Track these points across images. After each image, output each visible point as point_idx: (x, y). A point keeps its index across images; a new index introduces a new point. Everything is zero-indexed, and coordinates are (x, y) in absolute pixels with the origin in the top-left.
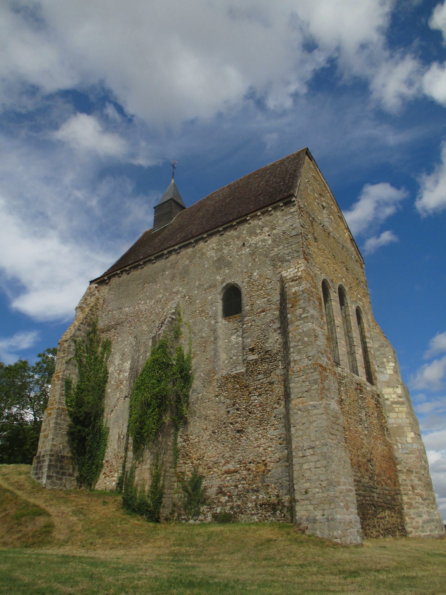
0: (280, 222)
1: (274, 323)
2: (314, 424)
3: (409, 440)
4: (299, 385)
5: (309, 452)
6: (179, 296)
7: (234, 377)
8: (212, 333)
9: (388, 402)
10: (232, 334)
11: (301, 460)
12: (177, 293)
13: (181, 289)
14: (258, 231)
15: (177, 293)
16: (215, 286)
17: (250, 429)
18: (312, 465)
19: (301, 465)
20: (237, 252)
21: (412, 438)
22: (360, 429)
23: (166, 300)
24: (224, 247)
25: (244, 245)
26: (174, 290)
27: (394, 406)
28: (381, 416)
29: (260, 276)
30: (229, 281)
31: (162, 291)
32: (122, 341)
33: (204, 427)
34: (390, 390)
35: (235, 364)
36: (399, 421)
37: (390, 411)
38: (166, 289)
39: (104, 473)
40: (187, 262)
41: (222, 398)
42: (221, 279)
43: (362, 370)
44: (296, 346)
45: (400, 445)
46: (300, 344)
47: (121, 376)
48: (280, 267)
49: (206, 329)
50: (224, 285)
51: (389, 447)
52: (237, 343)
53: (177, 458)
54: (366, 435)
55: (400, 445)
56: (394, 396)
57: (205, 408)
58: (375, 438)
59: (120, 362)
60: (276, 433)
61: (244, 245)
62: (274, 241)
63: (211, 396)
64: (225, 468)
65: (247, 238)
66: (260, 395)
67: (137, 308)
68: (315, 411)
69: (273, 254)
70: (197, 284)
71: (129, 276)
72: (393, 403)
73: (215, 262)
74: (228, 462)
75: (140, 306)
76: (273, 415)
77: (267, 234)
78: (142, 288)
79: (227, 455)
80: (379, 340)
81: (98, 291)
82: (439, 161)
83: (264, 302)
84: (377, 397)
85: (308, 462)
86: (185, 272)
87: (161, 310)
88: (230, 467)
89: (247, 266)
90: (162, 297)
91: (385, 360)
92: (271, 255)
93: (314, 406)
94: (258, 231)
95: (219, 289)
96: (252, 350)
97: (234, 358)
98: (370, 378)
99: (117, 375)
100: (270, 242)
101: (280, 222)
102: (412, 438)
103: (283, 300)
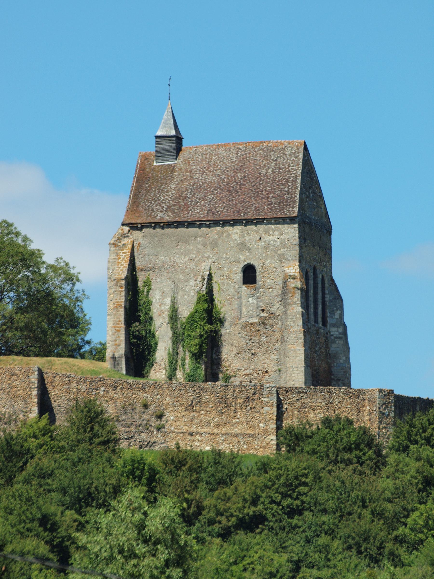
2: (298, 358)
3: (341, 361)
5: (295, 369)
7: (251, 324)
8: (236, 293)
9: (333, 338)
10: (249, 297)
11: (291, 373)
13: (211, 256)
14: (271, 233)
15: (208, 257)
18: (296, 375)
19: (291, 374)
20: (256, 243)
23: (199, 260)
25: (260, 239)
26: (206, 255)
28: (327, 346)
30: (249, 262)
31: (195, 252)
33: (231, 349)
34: (335, 329)
36: (338, 349)
37: (332, 343)
38: (198, 252)
42: (245, 258)
47: (163, 308)
50: (246, 263)
51: (330, 367)
52: (253, 303)
53: (175, 369)
56: (337, 333)
57: (231, 339)
58: (322, 360)
59: (160, 297)
60: (275, 357)
62: (281, 243)
66: (267, 337)
67: (172, 259)
68: (299, 352)
69: (280, 252)
70: (224, 256)
71: (163, 231)
72: (336, 338)
73: (239, 244)
74: (246, 370)
75: (175, 258)
76: (274, 348)
77: (277, 237)
78: (176, 245)
79: (246, 366)
80: (333, 295)
84: (327, 335)
88: (248, 372)
90: (196, 258)
91: (335, 309)
93: (299, 350)
94: (271, 233)
96: (263, 310)
98: (324, 323)
99: (158, 307)
100: (279, 243)
101: (287, 231)
102: (344, 360)
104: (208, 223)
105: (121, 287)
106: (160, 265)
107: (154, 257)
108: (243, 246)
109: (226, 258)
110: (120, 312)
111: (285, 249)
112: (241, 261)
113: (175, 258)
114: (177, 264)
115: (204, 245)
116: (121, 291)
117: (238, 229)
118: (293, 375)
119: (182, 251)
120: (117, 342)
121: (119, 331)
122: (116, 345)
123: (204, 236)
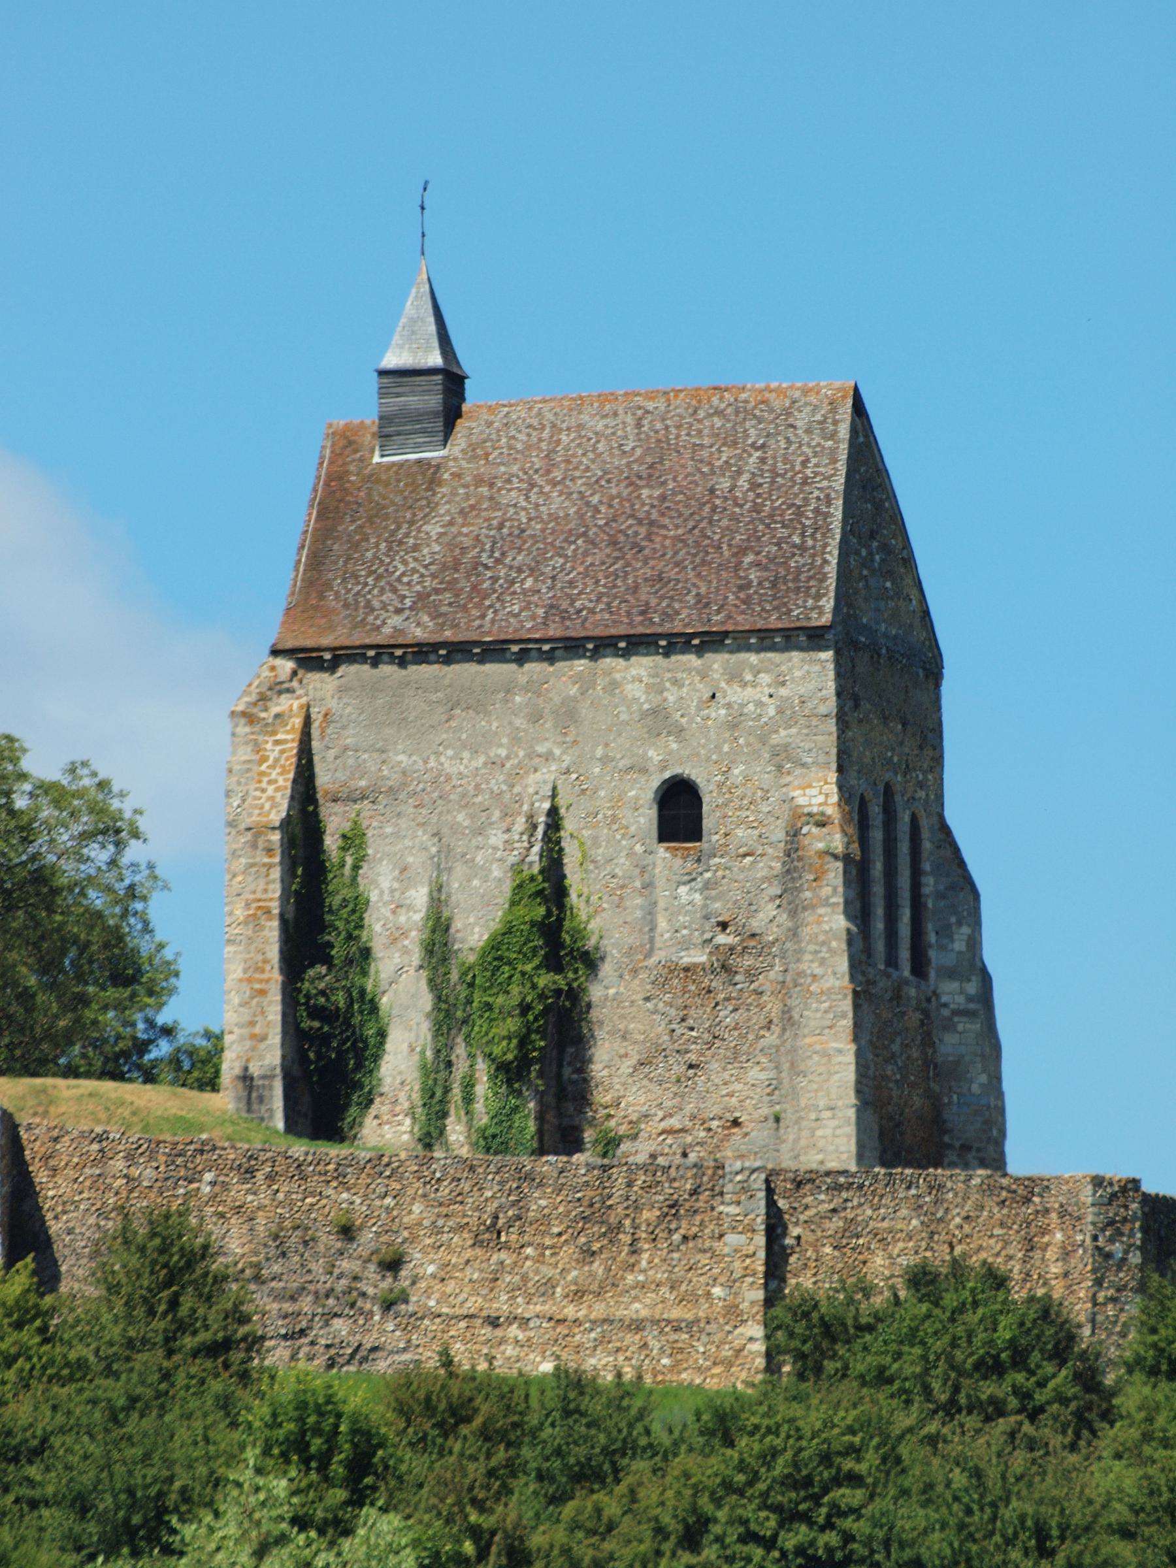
0: (798, 674)
1: (771, 884)
2: (836, 1077)
4: (819, 1015)
6: (553, 768)
9: (946, 1012)
10: (679, 884)
12: (548, 757)
13: (557, 752)
15: (548, 757)
16: (644, 771)
17: (715, 1065)
18: (829, 1132)
19: (813, 1131)
21: (981, 1085)
22: (889, 1073)
23: (520, 765)
24: (668, 685)
25: (713, 696)
26: (540, 749)
27: (956, 1019)
28: (928, 1041)
29: (747, 779)
30: (678, 770)
31: (505, 740)
32: (397, 835)
33: (622, 1051)
34: (954, 986)
35: (685, 945)
37: (945, 1028)
38: (516, 740)
39: (376, 1117)
40: (573, 690)
41: (661, 1005)
42: (663, 759)
43: (905, 954)
44: (816, 952)
45: (955, 1097)
46: (824, 949)
48: (789, 773)
49: (622, 860)
54: (897, 1081)
55: (955, 1097)
56: (960, 999)
58: (912, 1085)
59: (396, 885)
61: (713, 696)
62: (780, 711)
63: (639, 997)
64: (663, 1125)
65: (723, 684)
67: (432, 763)
68: (840, 1059)
69: (775, 739)
70: (599, 752)
72: (956, 1013)
73: (644, 715)
74: (671, 1115)
75: (442, 759)
77: (767, 691)
78: (444, 717)
80: (948, 875)
81: (301, 682)
82: (962, 888)
83: (750, 836)
84: (928, 1007)
85: (825, 1127)
86: (568, 715)
87: (504, 787)
88: (675, 1122)
89: (718, 747)
90: (508, 757)
92: (772, 742)
94: (749, 677)
95: (655, 783)
96: (724, 926)
97: (685, 932)
98: (919, 966)
99: (389, 914)
100: (772, 712)
102: (981, 1085)
103: (688, 643)
104: (546, 647)
105: (269, 851)
106: (394, 780)
107: (375, 755)
108: (658, 720)
109: (605, 760)
110: (266, 932)
111: (794, 731)
112: (652, 769)
113: (442, 759)
114: (449, 778)
115: (536, 717)
116: (270, 866)
117: (641, 666)
118: (819, 1133)
119: (464, 736)
120: (257, 1030)
121: (262, 992)
122: (253, 1036)
123: (535, 688)
